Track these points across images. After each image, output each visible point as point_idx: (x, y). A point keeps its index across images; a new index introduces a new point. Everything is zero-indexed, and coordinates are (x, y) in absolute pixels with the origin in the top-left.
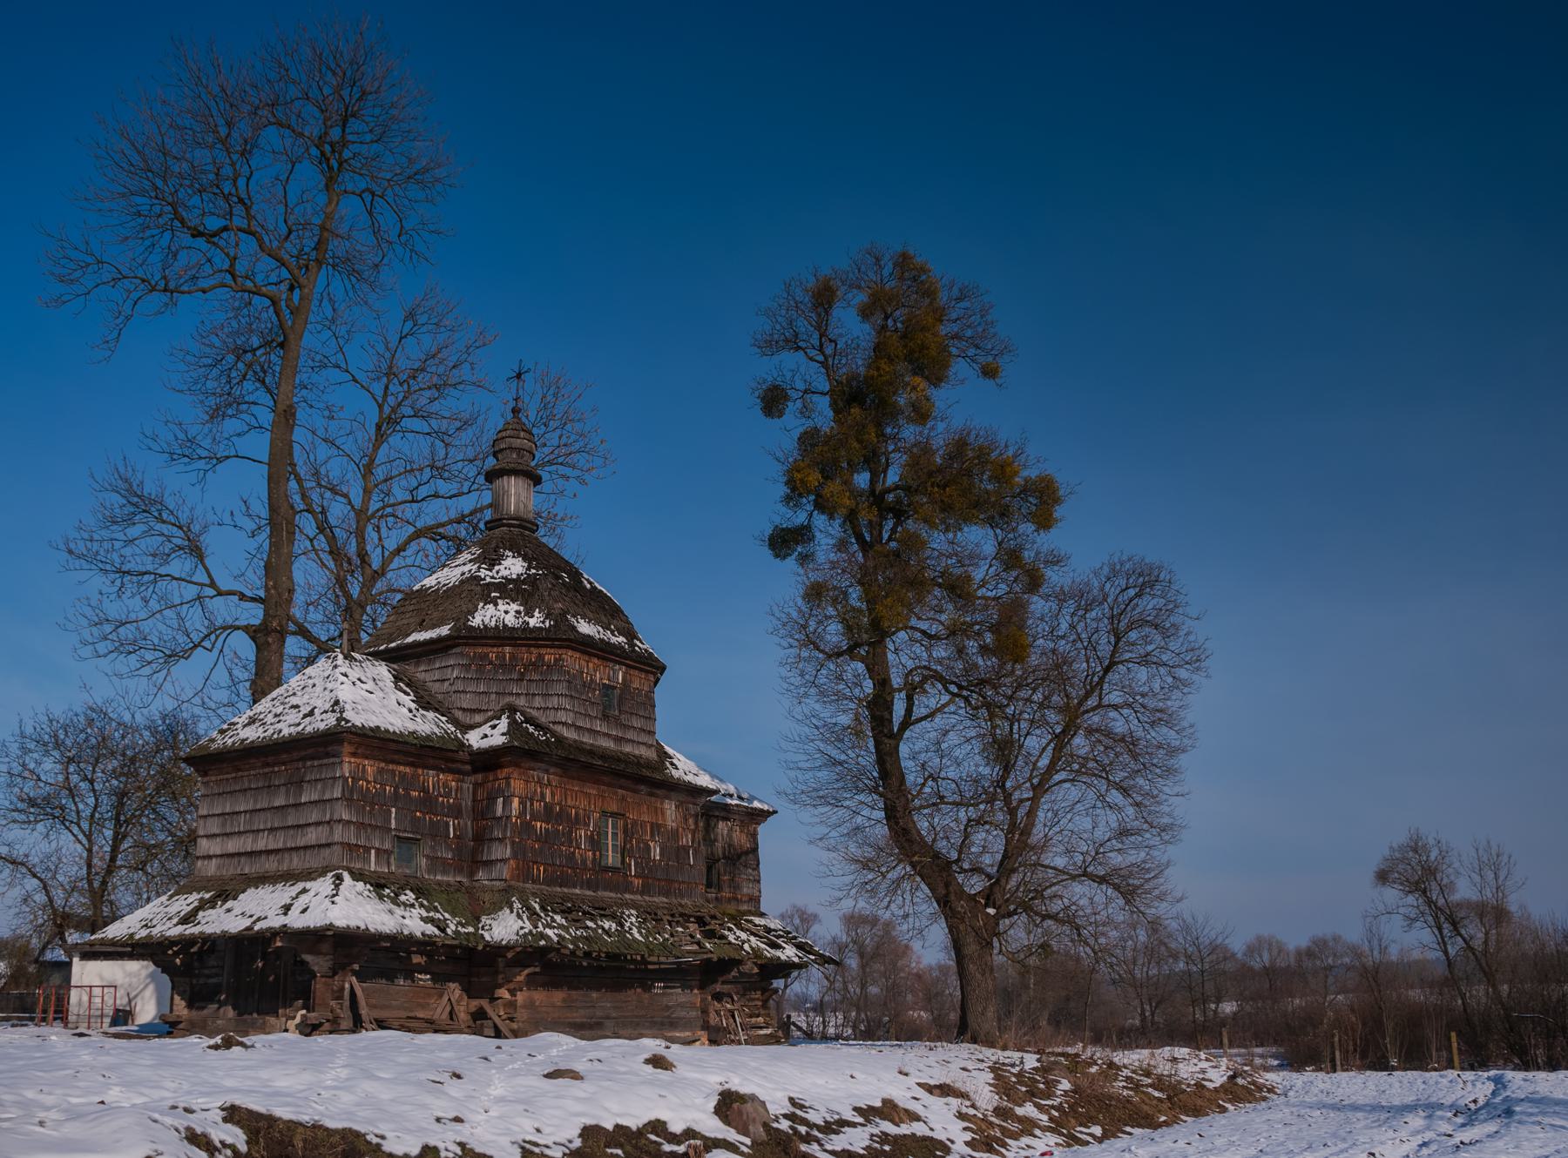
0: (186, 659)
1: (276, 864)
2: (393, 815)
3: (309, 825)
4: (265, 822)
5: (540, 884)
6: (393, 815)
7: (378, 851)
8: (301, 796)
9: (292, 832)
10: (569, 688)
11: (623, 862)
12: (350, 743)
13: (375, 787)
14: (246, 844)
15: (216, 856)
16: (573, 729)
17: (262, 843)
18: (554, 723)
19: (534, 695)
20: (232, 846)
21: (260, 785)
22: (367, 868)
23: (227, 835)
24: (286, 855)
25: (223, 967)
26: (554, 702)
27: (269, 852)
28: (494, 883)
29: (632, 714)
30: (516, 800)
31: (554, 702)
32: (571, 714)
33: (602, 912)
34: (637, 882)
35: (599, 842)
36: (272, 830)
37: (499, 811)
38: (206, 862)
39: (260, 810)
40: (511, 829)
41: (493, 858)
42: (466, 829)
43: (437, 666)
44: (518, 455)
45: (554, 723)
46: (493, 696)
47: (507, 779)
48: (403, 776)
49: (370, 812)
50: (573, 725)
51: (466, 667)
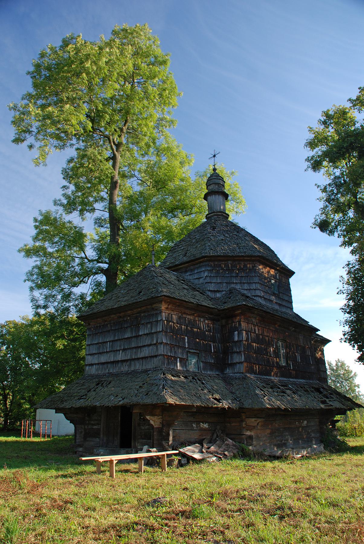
0: (77, 287)
1: (127, 367)
2: (186, 341)
3: (144, 346)
4: (120, 346)
5: (257, 375)
6: (186, 341)
9: (134, 350)
10: (260, 280)
11: (287, 363)
12: (165, 302)
13: (177, 326)
14: (111, 358)
15: (96, 364)
17: (120, 356)
18: (255, 296)
19: (244, 283)
21: (117, 328)
23: (100, 353)
24: (133, 363)
25: (101, 420)
29: (283, 294)
30: (244, 332)
31: (254, 286)
35: (278, 353)
37: (236, 339)
38: (90, 368)
39: (117, 340)
40: (244, 347)
43: (196, 272)
44: (218, 186)
45: (255, 296)
46: (225, 284)
47: (239, 322)
48: (189, 321)
49: (176, 339)
51: (211, 271)
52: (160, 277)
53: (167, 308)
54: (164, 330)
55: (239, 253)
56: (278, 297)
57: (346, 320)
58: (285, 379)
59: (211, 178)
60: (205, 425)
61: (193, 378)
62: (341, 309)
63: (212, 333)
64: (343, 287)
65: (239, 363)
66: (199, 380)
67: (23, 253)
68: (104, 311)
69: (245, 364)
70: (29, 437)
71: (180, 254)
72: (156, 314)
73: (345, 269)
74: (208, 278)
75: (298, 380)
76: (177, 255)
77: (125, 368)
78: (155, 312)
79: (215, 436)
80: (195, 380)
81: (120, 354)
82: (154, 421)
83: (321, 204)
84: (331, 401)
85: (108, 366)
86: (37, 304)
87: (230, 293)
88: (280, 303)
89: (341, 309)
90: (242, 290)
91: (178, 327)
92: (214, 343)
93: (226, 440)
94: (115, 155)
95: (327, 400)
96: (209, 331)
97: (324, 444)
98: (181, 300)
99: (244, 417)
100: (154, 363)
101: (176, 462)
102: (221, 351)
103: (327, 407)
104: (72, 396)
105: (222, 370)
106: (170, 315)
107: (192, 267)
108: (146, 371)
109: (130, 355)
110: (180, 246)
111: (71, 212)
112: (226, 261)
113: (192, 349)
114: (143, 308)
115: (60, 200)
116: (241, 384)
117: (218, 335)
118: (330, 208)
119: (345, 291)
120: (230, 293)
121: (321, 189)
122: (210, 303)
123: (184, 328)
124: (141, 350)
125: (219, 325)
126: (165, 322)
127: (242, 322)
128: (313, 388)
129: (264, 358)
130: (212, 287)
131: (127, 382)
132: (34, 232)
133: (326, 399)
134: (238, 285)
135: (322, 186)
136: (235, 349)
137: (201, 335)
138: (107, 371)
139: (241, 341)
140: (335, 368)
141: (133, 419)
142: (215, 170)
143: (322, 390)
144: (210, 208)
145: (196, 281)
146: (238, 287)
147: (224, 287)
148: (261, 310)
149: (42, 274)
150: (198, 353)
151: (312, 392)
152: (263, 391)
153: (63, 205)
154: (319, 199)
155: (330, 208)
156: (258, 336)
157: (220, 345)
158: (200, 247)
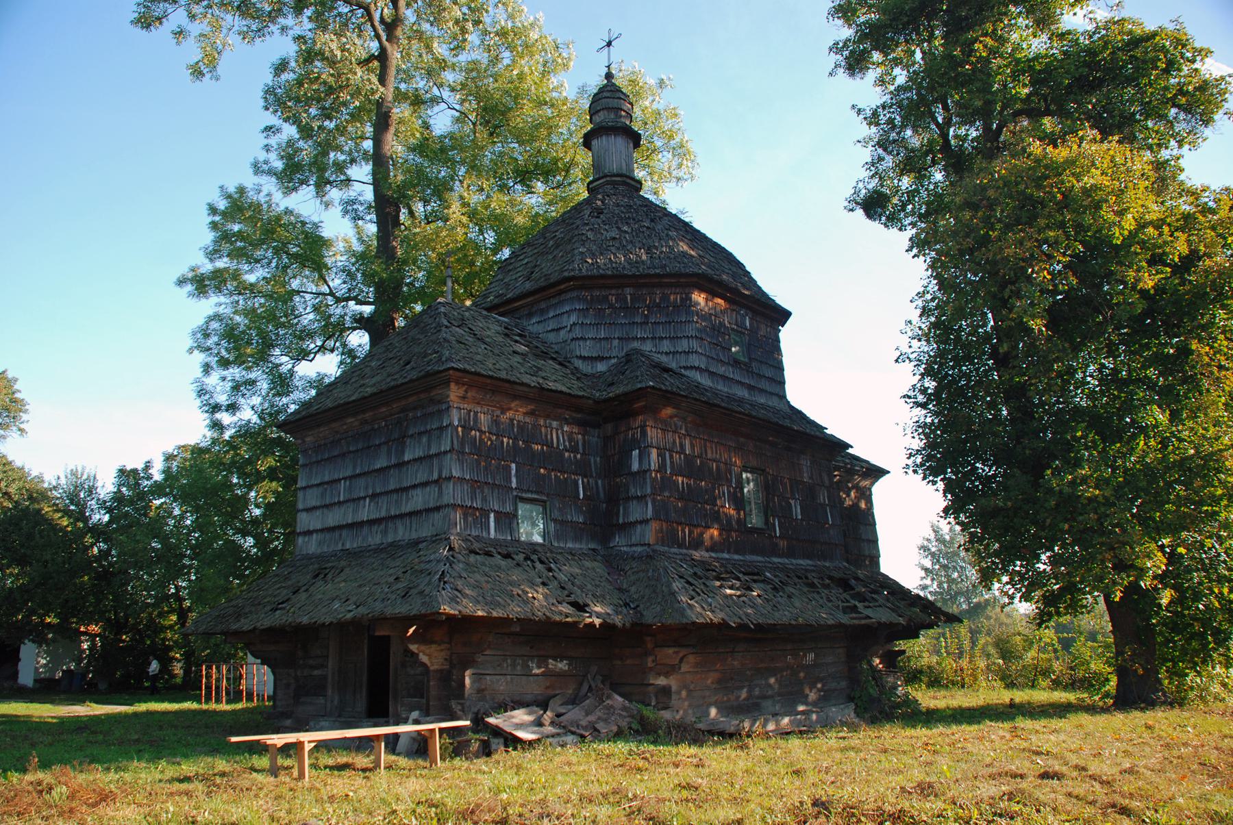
1: (379, 536)
2: (513, 472)
3: (414, 487)
6: (513, 472)
7: (496, 512)
8: (403, 453)
9: (395, 496)
11: (767, 522)
12: (457, 383)
13: (490, 439)
15: (317, 531)
16: (706, 374)
17: (366, 512)
18: (686, 368)
19: (661, 338)
20: (334, 518)
21: (360, 446)
22: (484, 534)
24: (390, 525)
25: (327, 657)
26: (684, 345)
27: (371, 522)
28: (634, 549)
29: (761, 362)
30: (654, 453)
31: (684, 345)
32: (704, 359)
33: (755, 578)
34: (783, 544)
36: (374, 496)
37: (635, 467)
38: (306, 539)
39: (359, 475)
41: (632, 519)
42: (597, 488)
43: (551, 314)
45: (686, 368)
46: (616, 342)
47: (643, 428)
49: (486, 468)
50: (707, 370)
52: (458, 327)
53: (464, 398)
54: (456, 447)
55: (649, 268)
56: (748, 371)
57: (917, 422)
58: (760, 559)
59: (600, 96)
60: (560, 665)
61: (527, 558)
62: (904, 397)
63: (582, 455)
64: (910, 347)
65: (641, 522)
66: (542, 562)
67: (189, 288)
68: (330, 409)
69: (654, 525)
70: (218, 701)
71: (519, 274)
72: (440, 412)
73: (914, 305)
74: (577, 327)
75: (794, 561)
76: (514, 277)
77: (375, 538)
78: (436, 408)
79: (585, 687)
80: (533, 561)
81: (364, 507)
82: (430, 657)
83: (866, 154)
84: (869, 607)
85: (341, 535)
86: (212, 401)
87: (628, 361)
88: (752, 384)
89: (904, 397)
90: (656, 355)
91: (492, 441)
92: (586, 477)
93: (609, 697)
94: (383, 50)
95: (859, 605)
96: (574, 449)
97: (856, 704)
98: (496, 379)
99: (650, 646)
100: (433, 525)
101: (475, 746)
102: (602, 495)
103: (856, 622)
104: (259, 604)
105: (605, 539)
106: (472, 414)
107: (543, 305)
108: (415, 544)
109: (385, 508)
110: (521, 257)
111: (295, 189)
112: (619, 287)
113: (528, 491)
114: (411, 400)
115: (266, 162)
116: (643, 571)
117: (595, 461)
118: (889, 161)
119: (915, 355)
120: (628, 361)
121: (865, 118)
122: (576, 384)
123: (508, 443)
124: (407, 495)
125: (598, 437)
126: (460, 429)
127: (649, 429)
128: (830, 578)
129: (706, 510)
130: (585, 349)
131: (373, 569)
132: (208, 237)
133: (857, 603)
134: (648, 342)
135: (868, 112)
136: (632, 491)
137: (553, 458)
138: (340, 547)
139: (645, 472)
140: (947, 538)
141: (391, 655)
142: (609, 76)
143: (853, 582)
144: (596, 165)
145: (551, 337)
146: (647, 347)
147: (617, 350)
148: (696, 400)
149: (231, 334)
150: (545, 502)
151: (827, 587)
152: (691, 584)
153: (275, 174)
154: (864, 142)
155: (889, 161)
156: (689, 460)
157: (600, 482)
158: (562, 256)
